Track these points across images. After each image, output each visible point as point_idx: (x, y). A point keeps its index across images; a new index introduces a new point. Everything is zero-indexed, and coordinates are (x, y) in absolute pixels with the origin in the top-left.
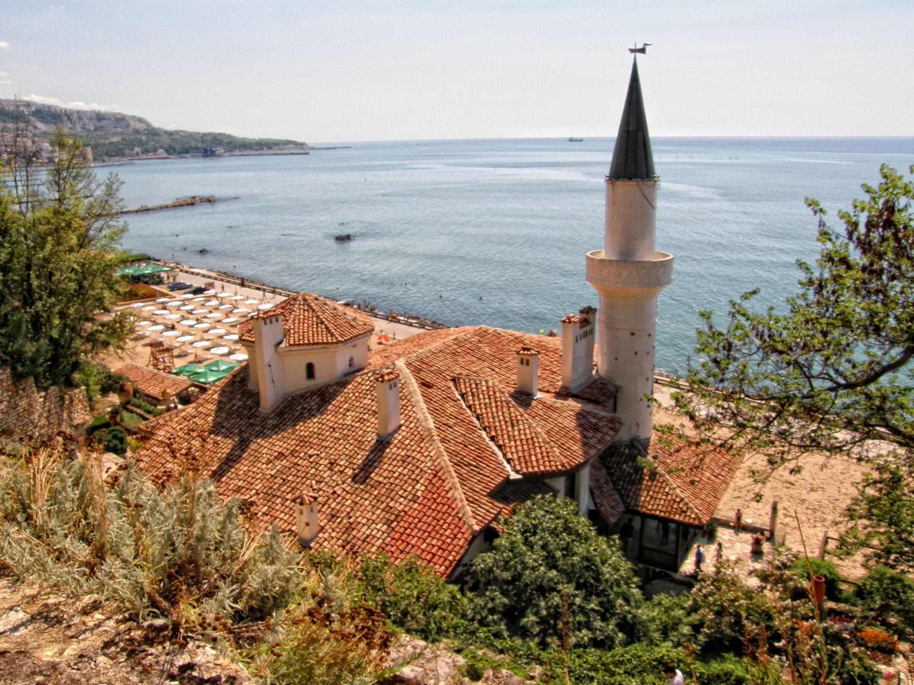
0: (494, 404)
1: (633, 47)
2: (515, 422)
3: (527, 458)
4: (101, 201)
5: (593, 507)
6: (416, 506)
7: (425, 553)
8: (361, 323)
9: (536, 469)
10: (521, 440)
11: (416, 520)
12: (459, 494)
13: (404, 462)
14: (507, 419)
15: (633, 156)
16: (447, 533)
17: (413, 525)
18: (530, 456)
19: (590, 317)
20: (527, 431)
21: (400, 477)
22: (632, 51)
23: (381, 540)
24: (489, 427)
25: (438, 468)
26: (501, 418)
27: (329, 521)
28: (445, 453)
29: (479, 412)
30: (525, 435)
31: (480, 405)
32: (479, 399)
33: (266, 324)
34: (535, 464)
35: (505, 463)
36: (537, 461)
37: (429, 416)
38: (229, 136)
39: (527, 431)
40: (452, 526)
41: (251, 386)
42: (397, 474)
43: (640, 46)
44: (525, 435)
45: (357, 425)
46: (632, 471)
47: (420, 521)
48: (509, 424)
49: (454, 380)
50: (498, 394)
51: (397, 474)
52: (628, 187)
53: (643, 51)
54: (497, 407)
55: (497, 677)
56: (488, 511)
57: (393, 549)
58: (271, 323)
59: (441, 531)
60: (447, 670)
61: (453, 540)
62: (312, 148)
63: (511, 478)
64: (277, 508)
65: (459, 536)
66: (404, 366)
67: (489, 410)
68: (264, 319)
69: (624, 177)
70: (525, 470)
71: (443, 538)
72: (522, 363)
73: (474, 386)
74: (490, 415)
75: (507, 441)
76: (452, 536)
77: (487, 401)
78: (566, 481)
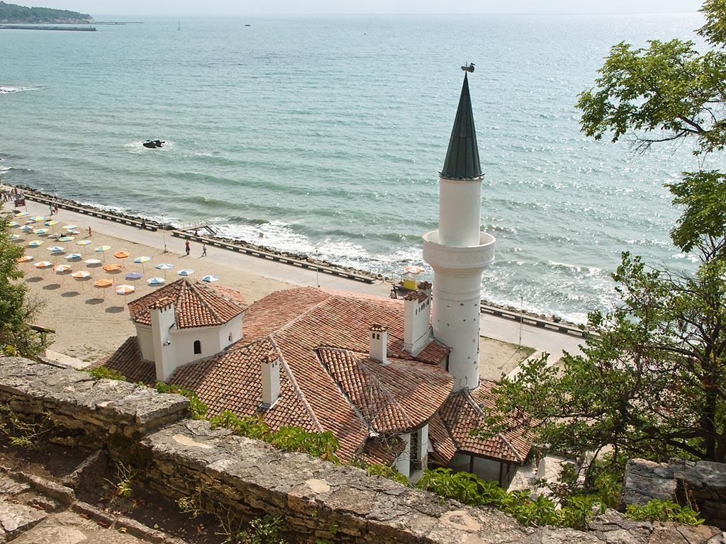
4: (144, 363)
19: (426, 292)
41: (146, 356)
49: (317, 351)
58: (166, 310)
68: (161, 308)
69: (455, 177)
73: (334, 356)
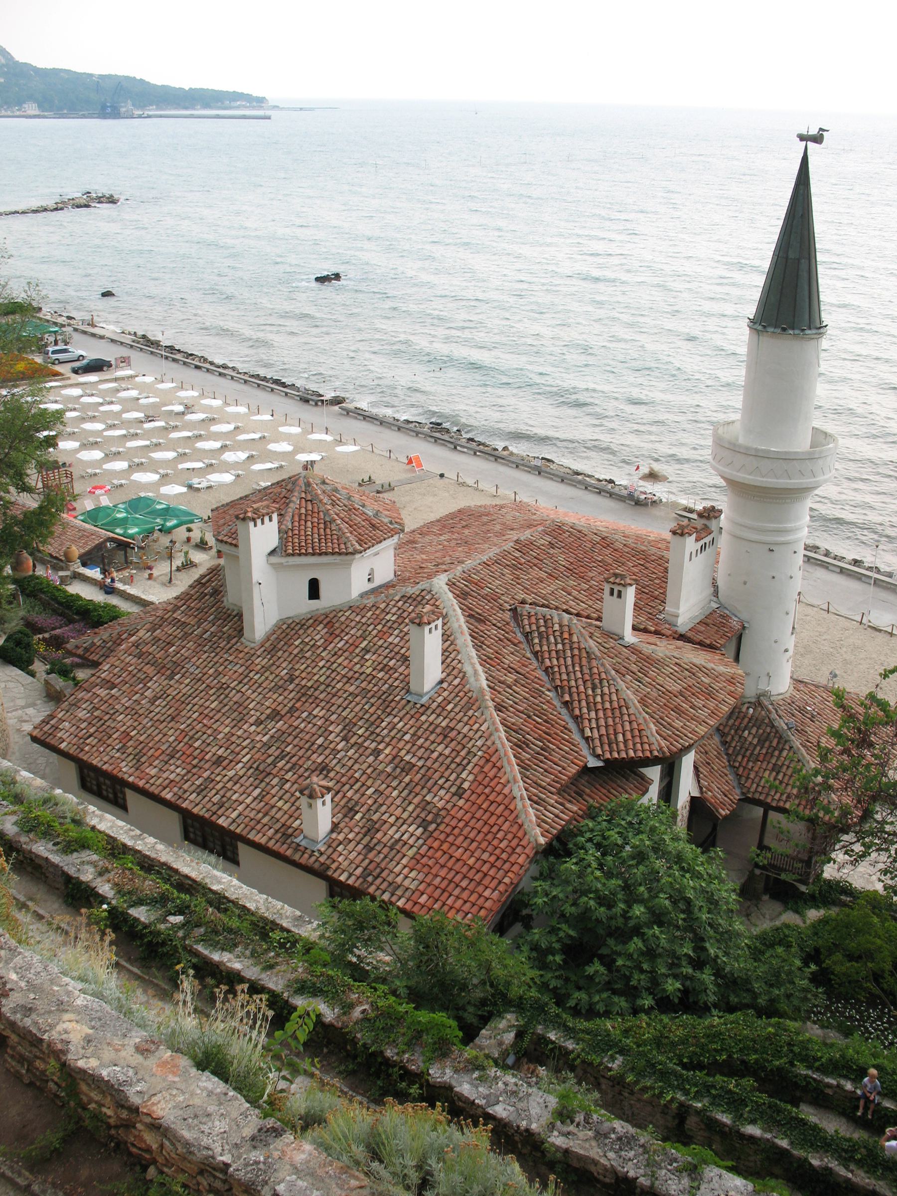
0: (569, 653)
3: (612, 737)
5: (696, 794)
6: (461, 803)
7: (473, 871)
8: (386, 520)
9: (624, 755)
10: (605, 710)
11: (461, 824)
12: (519, 789)
13: (446, 736)
14: (587, 677)
15: (789, 300)
16: (501, 845)
17: (456, 831)
18: (616, 734)
20: (614, 697)
21: (441, 759)
22: (802, 138)
23: (414, 849)
24: (562, 687)
25: (491, 751)
26: (579, 675)
27: (345, 816)
28: (501, 727)
30: (611, 702)
31: (550, 652)
33: (255, 525)
34: (622, 746)
35: (583, 744)
36: (625, 741)
37: (480, 669)
38: (142, 81)
39: (614, 697)
40: (510, 836)
42: (435, 755)
43: (814, 131)
44: (611, 702)
45: (380, 675)
46: (755, 741)
47: (466, 825)
48: (589, 684)
51: (435, 755)
52: (781, 346)
53: (818, 139)
54: (573, 656)
55: (588, 1123)
56: (557, 816)
57: (430, 863)
58: (263, 523)
59: (495, 842)
60: (538, 1110)
61: (510, 855)
62: (275, 107)
63: (590, 765)
64: (273, 791)
65: (518, 850)
66: (446, 588)
67: (562, 661)
70: (608, 756)
71: (498, 852)
74: (563, 669)
75: (585, 710)
76: (509, 850)
77: (560, 647)
78: (662, 771)
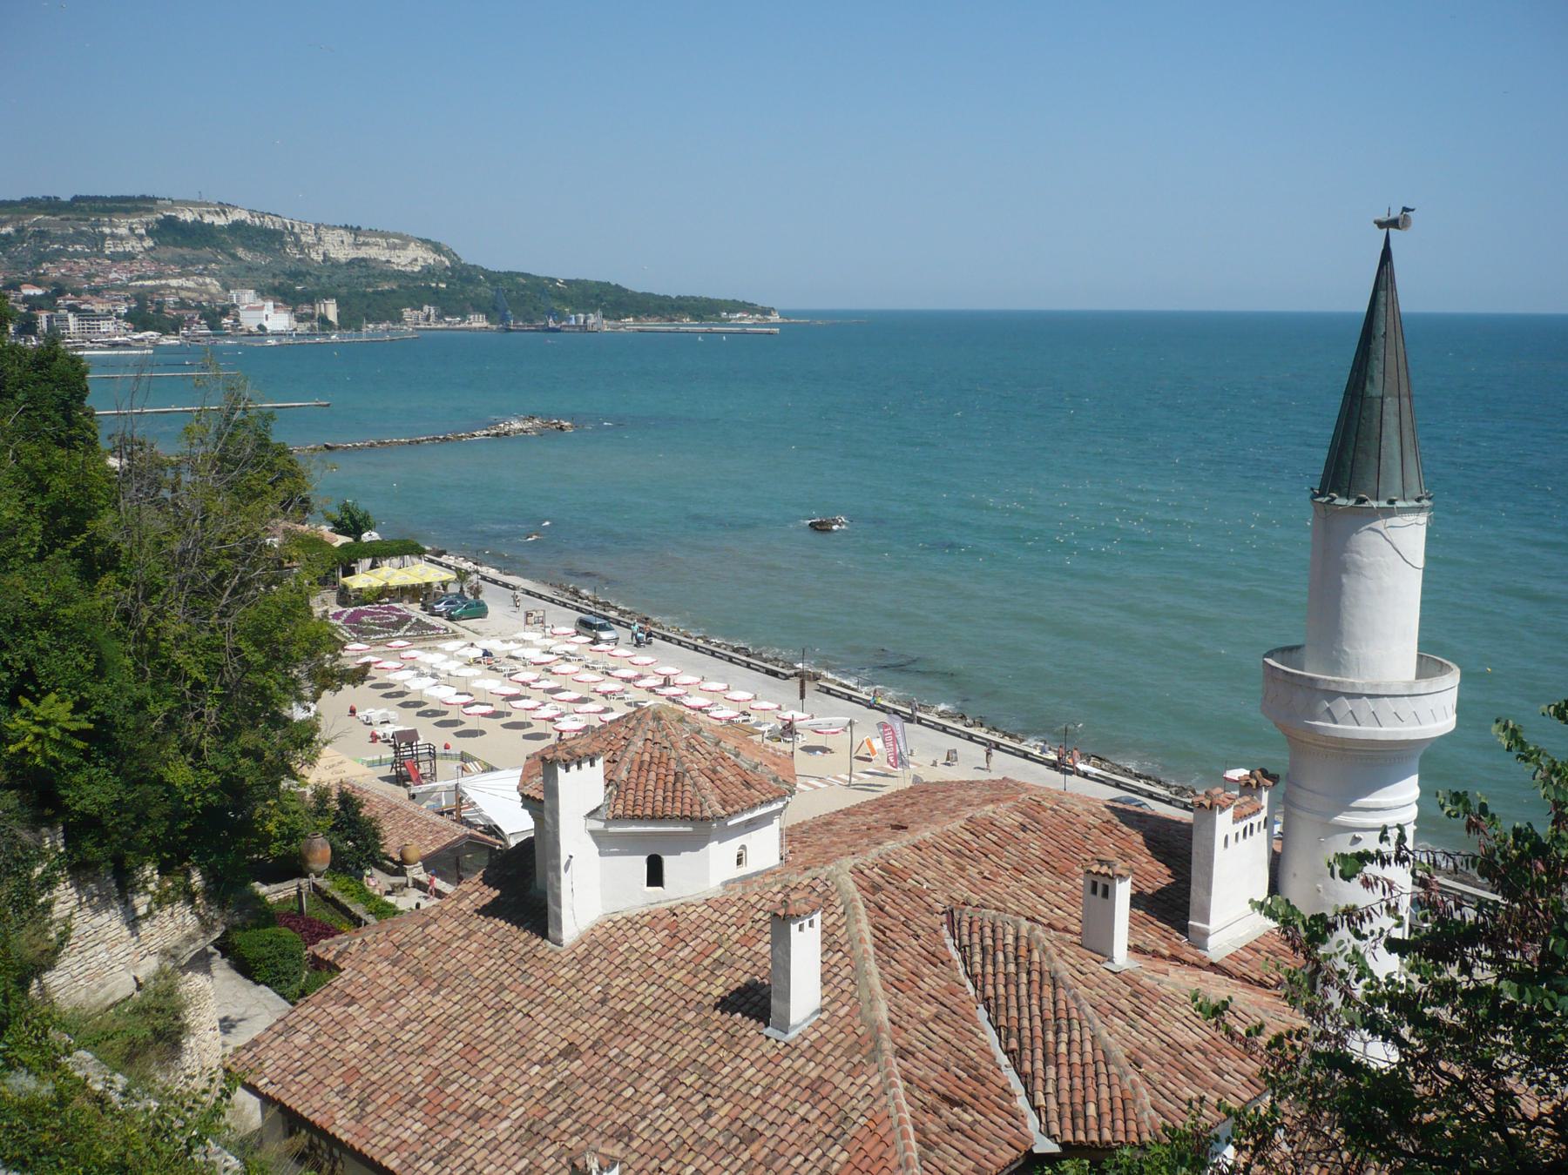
1: (1384, 217)
2: (1064, 1022)
9: (1094, 1137)
13: (815, 1092)
22: (1381, 225)
28: (901, 1084)
29: (990, 991)
32: (994, 964)
50: (1036, 957)
63: (1036, 1150)
70: (1069, 1137)
72: (1094, 891)
